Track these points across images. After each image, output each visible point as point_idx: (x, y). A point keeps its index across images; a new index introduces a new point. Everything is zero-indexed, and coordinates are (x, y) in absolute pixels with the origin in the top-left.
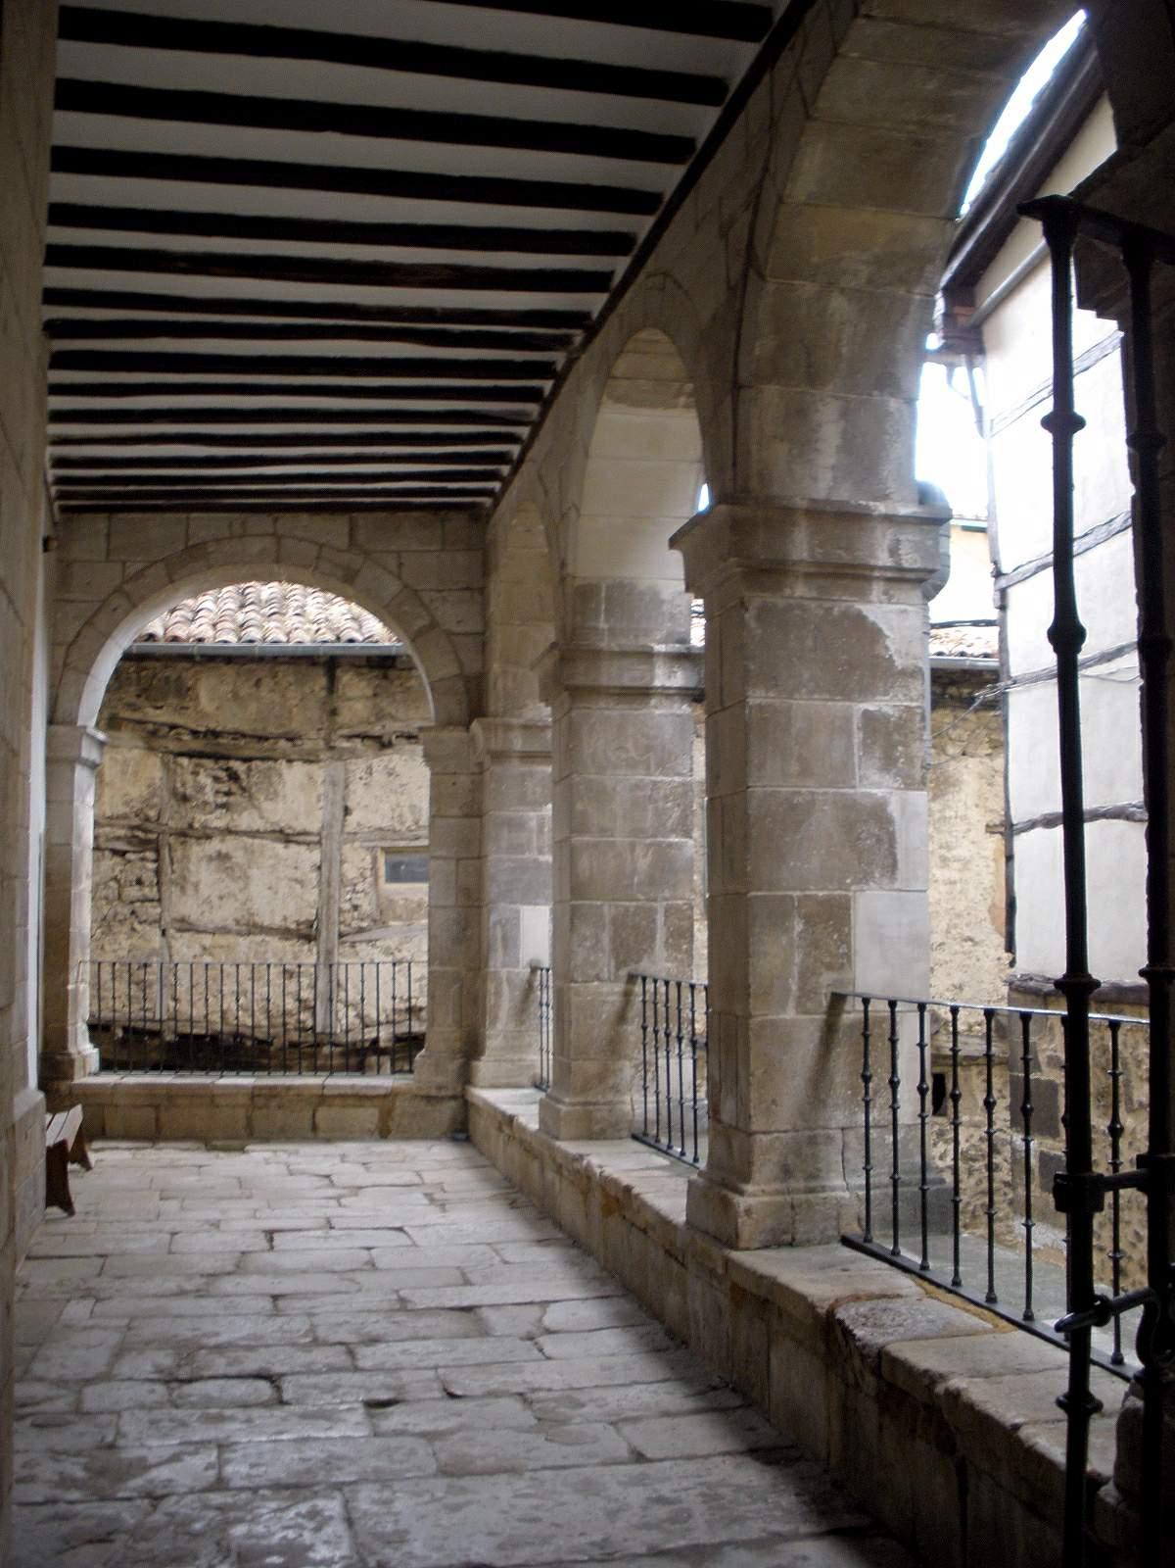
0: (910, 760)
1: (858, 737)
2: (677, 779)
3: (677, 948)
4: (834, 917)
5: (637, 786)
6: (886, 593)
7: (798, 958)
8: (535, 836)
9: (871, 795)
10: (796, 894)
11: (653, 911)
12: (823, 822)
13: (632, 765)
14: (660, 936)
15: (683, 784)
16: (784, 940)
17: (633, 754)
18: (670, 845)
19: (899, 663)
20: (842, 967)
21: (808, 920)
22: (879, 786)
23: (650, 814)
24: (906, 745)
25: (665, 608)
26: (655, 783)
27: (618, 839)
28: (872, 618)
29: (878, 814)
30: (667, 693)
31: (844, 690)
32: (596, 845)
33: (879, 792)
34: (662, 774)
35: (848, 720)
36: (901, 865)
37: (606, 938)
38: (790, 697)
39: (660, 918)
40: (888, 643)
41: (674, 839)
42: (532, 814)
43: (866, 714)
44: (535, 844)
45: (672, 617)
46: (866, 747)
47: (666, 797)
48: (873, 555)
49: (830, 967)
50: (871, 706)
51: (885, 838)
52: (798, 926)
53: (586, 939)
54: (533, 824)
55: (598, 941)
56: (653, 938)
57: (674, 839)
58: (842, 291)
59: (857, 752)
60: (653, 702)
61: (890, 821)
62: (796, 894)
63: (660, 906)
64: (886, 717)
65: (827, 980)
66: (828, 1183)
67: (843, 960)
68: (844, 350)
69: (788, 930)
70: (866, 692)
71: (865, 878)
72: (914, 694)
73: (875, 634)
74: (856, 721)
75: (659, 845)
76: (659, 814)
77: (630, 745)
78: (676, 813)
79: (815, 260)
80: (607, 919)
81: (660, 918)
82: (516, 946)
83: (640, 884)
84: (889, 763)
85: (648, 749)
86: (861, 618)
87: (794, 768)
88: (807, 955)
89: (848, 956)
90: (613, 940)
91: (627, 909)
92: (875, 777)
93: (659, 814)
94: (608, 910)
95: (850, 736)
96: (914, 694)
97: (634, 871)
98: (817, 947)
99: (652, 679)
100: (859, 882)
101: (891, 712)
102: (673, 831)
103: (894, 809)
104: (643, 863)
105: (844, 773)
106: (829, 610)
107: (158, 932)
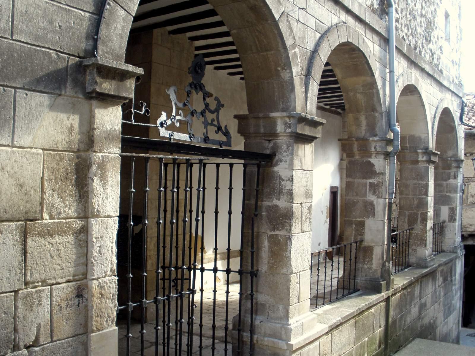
0: (379, 192)
1: (368, 187)
2: (425, 182)
3: (423, 223)
4: (361, 225)
5: (415, 184)
6: (375, 156)
7: (354, 232)
8: (445, 188)
9: (370, 200)
10: (354, 219)
11: (417, 214)
12: (360, 205)
13: (414, 179)
14: (419, 220)
15: (426, 183)
16: (351, 229)
17: (414, 176)
18: (423, 198)
19: (377, 172)
20: (362, 235)
21: (356, 225)
22: (372, 197)
23: (418, 191)
24: (378, 189)
25: (423, 141)
26: (419, 183)
27: (410, 196)
28: (372, 162)
29: (372, 204)
30: (422, 161)
31: (365, 178)
32: (405, 198)
33: (372, 199)
34: (421, 181)
35: (366, 184)
36: (376, 215)
37: (406, 220)
38: (354, 179)
39: (419, 215)
40: (376, 167)
41: (423, 197)
42: (445, 183)
43: (370, 183)
44: (445, 190)
45: (424, 142)
46: (370, 190)
47: (422, 187)
48: (371, 149)
49: (360, 235)
50: (371, 181)
51: (372, 208)
52: (354, 226)
53: (402, 219)
54: (445, 185)
55: (405, 220)
56: (417, 220)
57: (423, 197)
58: (358, 93)
59: (368, 190)
60: (420, 163)
61: (374, 205)
62: (354, 219)
63: (420, 213)
64: (374, 183)
65: (359, 238)
66: (74, 269)
67: (362, 234)
68: (363, 105)
69: (352, 227)
70: (370, 178)
71: (368, 217)
72: (380, 178)
73: (373, 165)
74: (368, 184)
75: (420, 198)
76: (420, 191)
77: (413, 174)
78: (424, 190)
79: (350, 88)
80: (407, 215)
81: (419, 215)
82: (440, 217)
83: (415, 207)
84: (374, 193)
85: (418, 175)
86: (370, 162)
87: (355, 194)
88: (355, 232)
89: (364, 233)
90: (408, 220)
91: (411, 213)
92: (371, 196)
93: (420, 191)
94: (407, 213)
95: (366, 187)
96: (380, 178)
97: (414, 204)
98: (358, 230)
99: (418, 158)
100: (367, 218)
101: (375, 182)
102: (423, 195)
103: (375, 203)
104: (416, 202)
105: (365, 195)
106: (363, 161)
107: (395, 205)
